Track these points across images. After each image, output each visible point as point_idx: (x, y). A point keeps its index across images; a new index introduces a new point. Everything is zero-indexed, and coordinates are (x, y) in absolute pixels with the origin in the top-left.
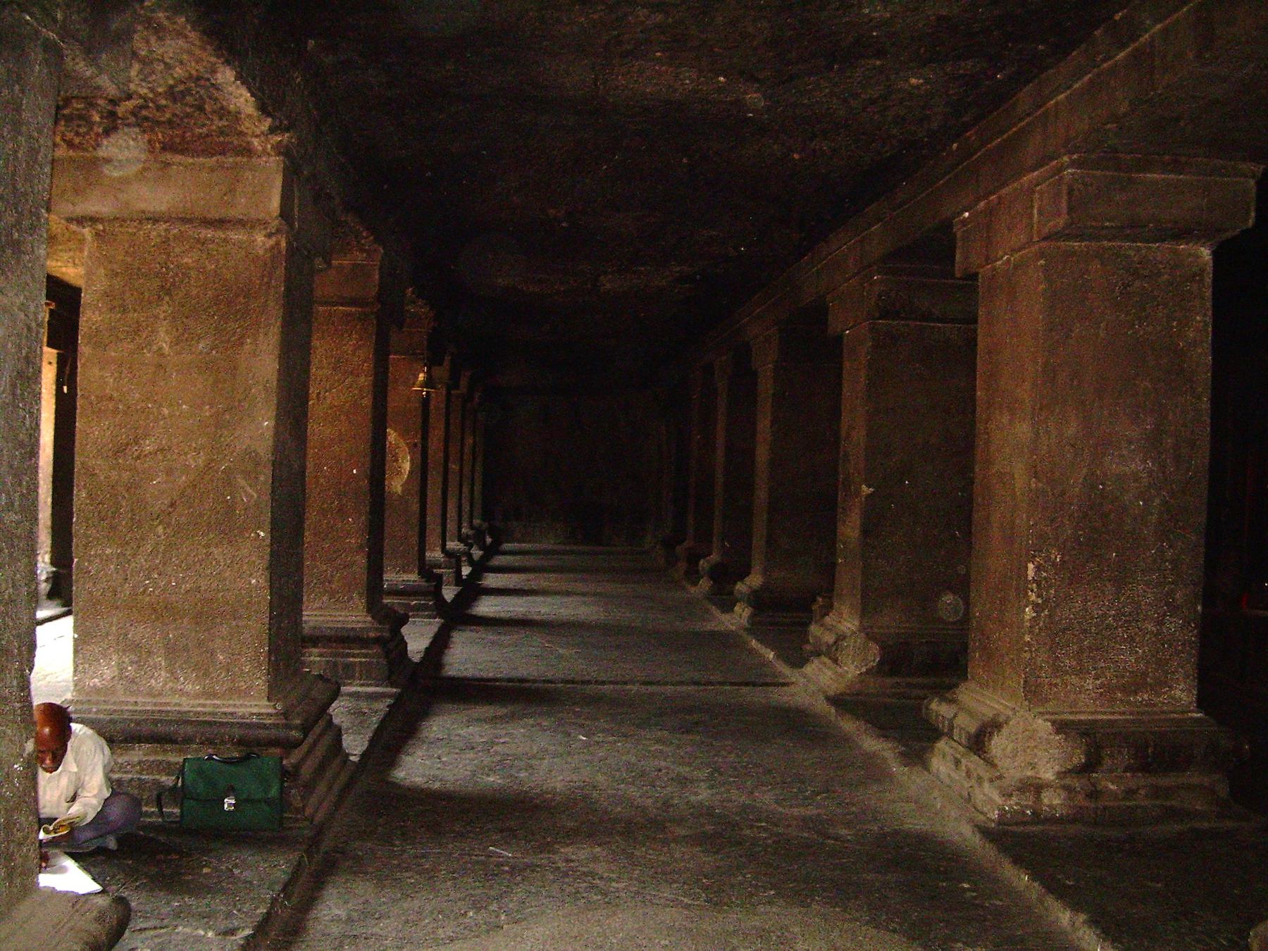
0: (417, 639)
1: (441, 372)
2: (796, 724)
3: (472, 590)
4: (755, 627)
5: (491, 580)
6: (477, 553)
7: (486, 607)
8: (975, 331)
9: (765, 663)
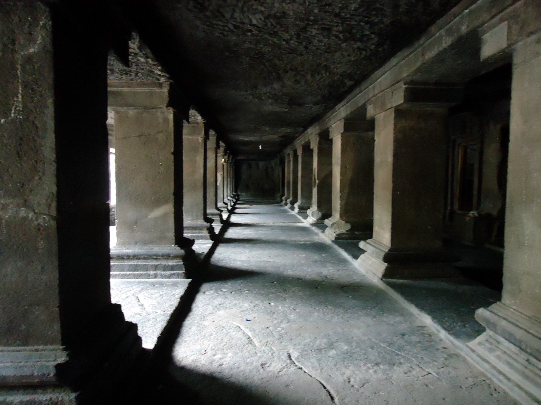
0: (225, 216)
1: (226, 157)
2: (304, 229)
3: (234, 208)
4: (299, 213)
5: (237, 206)
6: (234, 200)
7: (237, 211)
8: (508, 39)
9: (299, 219)
